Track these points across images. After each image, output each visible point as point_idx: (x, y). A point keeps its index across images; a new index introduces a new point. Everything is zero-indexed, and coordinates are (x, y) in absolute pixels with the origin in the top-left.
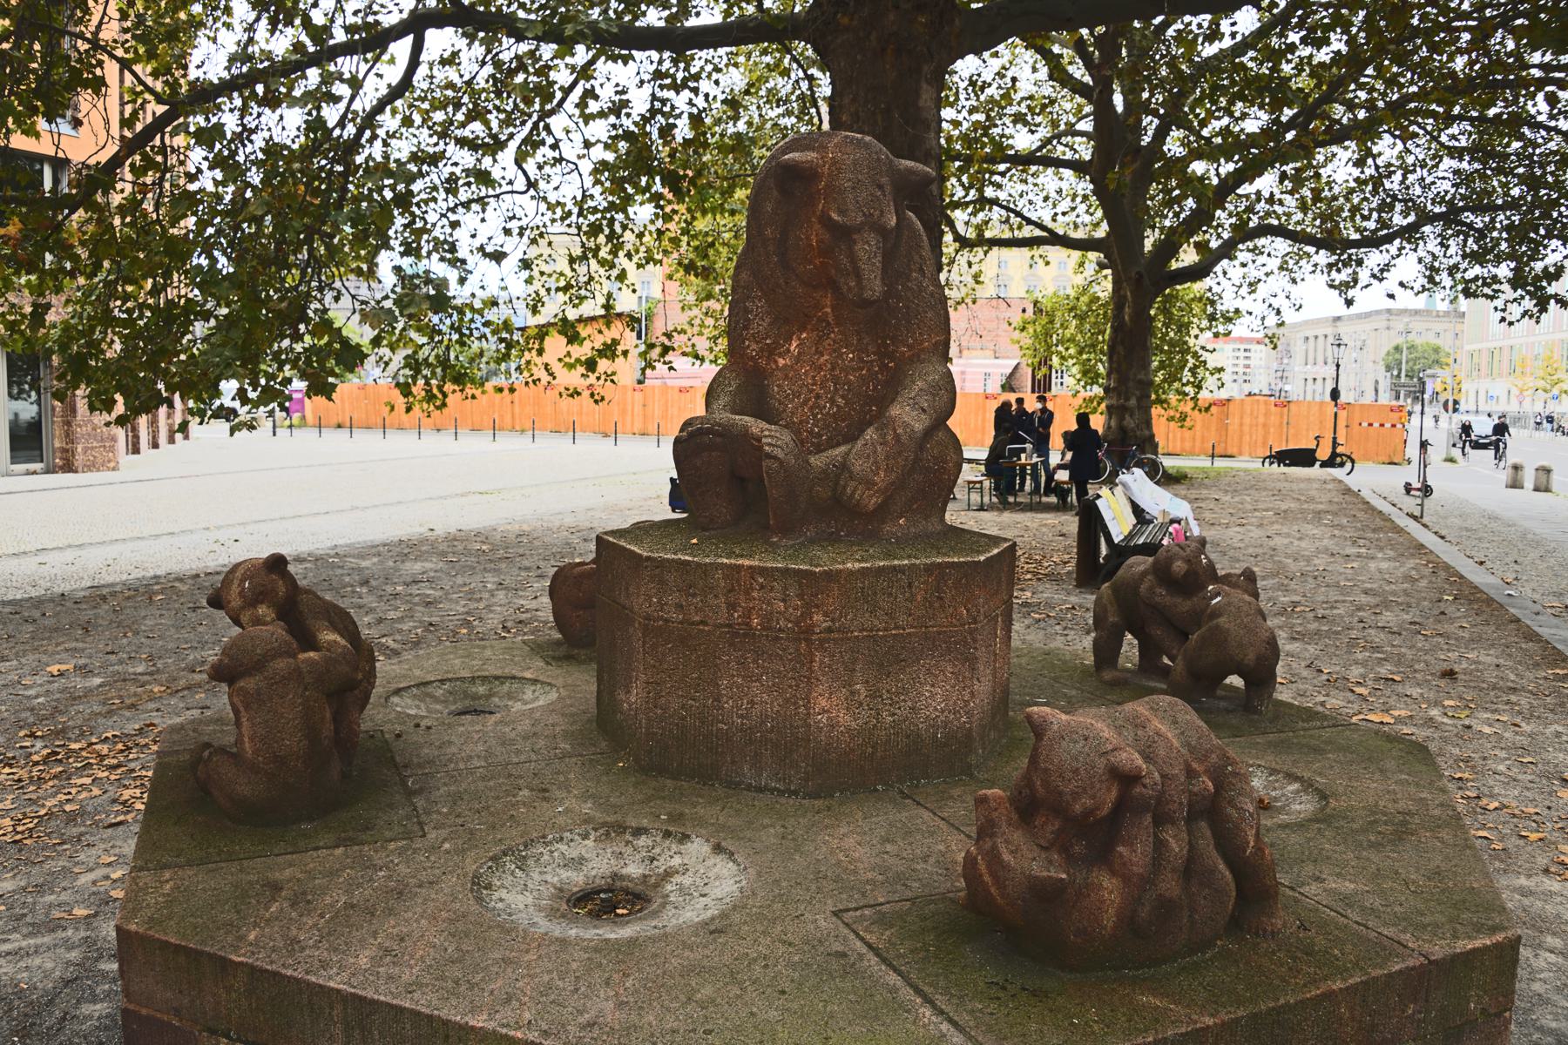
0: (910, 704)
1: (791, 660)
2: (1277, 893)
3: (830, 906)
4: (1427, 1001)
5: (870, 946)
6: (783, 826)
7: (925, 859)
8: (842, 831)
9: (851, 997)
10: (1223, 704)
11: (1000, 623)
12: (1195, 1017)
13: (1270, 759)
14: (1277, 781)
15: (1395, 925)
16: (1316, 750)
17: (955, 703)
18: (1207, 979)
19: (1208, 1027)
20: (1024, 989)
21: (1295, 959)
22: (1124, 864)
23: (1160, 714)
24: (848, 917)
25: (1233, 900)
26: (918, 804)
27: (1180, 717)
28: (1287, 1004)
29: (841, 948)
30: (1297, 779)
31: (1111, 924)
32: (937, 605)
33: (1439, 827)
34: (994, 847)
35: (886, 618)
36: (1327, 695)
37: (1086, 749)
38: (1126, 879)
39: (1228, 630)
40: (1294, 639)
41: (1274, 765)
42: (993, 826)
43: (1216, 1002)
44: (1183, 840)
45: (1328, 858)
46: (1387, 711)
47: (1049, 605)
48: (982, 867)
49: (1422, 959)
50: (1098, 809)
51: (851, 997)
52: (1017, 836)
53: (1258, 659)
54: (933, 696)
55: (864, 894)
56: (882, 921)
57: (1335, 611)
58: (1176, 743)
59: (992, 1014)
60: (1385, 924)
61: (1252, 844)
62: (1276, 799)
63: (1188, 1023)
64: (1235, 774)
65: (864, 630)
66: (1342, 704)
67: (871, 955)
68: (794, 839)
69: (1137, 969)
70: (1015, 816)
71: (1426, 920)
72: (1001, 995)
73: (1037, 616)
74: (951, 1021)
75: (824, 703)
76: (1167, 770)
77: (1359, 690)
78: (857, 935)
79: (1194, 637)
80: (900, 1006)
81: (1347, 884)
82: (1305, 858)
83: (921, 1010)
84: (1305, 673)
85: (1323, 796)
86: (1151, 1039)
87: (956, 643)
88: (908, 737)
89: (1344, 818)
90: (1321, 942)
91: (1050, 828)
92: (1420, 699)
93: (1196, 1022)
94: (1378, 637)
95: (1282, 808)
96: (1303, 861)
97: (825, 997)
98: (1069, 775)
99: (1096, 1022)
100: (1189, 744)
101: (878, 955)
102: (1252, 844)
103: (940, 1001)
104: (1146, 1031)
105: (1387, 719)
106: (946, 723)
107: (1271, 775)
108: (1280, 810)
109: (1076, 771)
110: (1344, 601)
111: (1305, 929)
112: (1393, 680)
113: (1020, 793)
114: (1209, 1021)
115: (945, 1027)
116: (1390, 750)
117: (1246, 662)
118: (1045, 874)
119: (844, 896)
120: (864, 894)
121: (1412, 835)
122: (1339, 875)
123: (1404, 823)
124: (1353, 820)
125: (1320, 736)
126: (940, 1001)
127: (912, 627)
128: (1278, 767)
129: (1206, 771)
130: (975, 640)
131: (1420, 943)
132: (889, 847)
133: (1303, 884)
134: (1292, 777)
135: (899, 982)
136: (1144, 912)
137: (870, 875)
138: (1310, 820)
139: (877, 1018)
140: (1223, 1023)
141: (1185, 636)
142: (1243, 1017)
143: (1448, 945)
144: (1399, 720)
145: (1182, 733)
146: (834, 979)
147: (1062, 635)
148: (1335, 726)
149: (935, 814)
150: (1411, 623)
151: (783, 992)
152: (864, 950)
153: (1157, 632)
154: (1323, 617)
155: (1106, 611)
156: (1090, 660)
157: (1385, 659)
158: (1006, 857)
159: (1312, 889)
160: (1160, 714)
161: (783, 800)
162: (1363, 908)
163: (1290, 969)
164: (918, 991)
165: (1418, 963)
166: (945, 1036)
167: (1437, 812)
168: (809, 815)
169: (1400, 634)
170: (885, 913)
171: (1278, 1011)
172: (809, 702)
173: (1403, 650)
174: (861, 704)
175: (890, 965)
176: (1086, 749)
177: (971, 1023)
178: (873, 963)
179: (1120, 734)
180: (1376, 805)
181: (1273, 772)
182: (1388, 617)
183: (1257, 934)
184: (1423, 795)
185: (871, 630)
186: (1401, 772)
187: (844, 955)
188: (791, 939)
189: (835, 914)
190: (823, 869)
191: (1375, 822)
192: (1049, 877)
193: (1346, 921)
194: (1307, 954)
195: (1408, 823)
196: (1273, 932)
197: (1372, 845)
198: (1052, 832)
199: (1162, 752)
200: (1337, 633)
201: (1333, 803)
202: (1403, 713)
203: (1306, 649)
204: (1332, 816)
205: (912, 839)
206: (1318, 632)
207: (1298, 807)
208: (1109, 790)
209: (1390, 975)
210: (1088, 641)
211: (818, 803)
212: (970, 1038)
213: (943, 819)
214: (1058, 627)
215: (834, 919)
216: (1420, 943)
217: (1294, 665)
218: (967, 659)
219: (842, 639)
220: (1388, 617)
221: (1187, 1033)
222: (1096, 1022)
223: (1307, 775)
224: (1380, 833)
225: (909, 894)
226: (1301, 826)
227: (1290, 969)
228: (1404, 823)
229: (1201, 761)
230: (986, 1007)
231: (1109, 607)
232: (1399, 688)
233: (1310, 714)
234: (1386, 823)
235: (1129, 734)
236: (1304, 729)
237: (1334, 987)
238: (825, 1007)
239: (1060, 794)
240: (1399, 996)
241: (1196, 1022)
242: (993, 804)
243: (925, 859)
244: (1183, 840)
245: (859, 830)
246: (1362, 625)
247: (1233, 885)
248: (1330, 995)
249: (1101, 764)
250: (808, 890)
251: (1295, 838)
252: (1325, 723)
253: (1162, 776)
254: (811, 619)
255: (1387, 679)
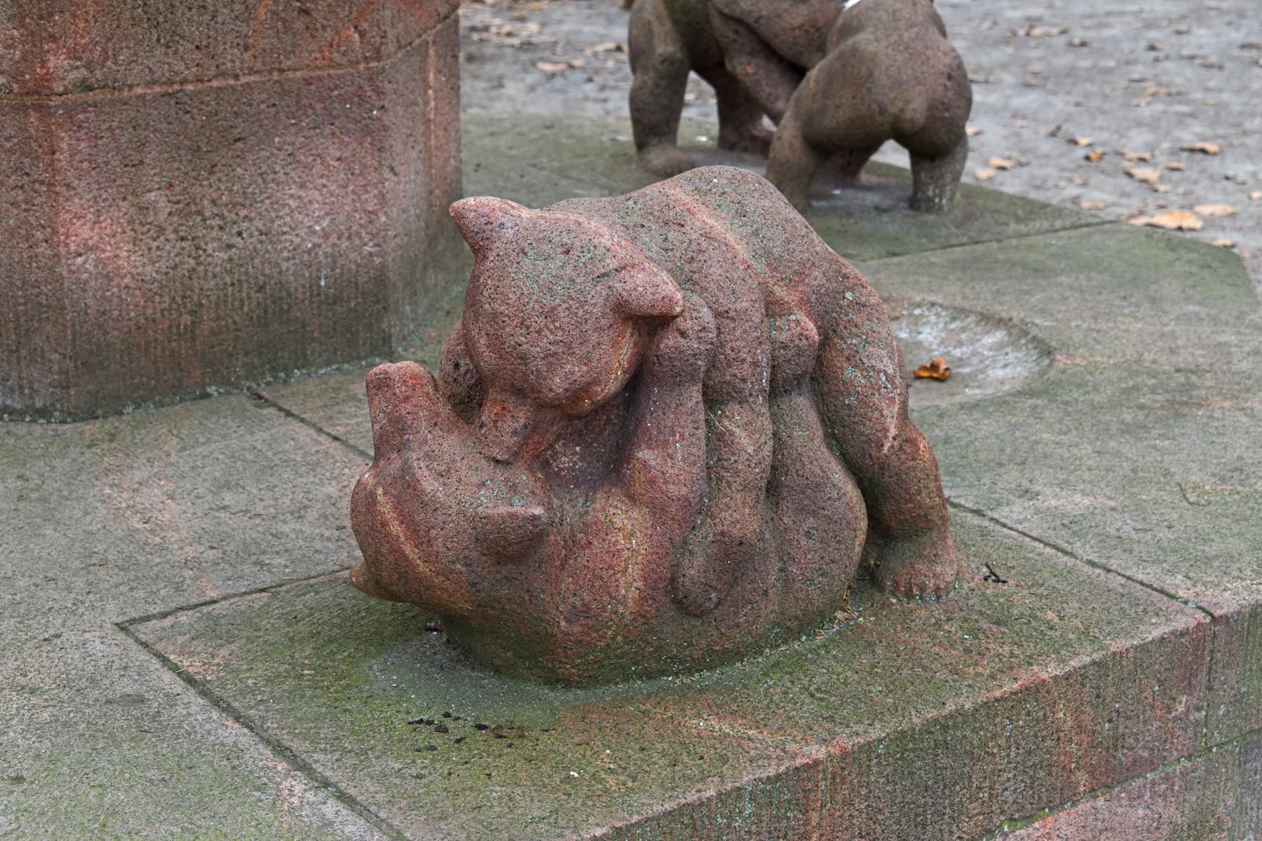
0: (259, 224)
1: (12, 151)
2: (944, 519)
3: (113, 614)
4: (1210, 688)
5: (190, 680)
6: (20, 477)
7: (299, 513)
8: (138, 475)
9: (153, 774)
10: (872, 199)
11: (432, 59)
12: (792, 747)
13: (953, 292)
14: (963, 329)
15: (1157, 561)
16: (1038, 271)
17: (349, 217)
18: (817, 680)
19: (817, 763)
20: (480, 727)
21: (975, 633)
22: (652, 482)
23: (713, 199)
24: (146, 631)
25: (862, 536)
26: (289, 414)
27: (751, 203)
28: (959, 712)
29: (131, 688)
30: (1001, 322)
31: (633, 593)
32: (299, 25)
33: (1248, 390)
34: (406, 469)
35: (197, 55)
36: (1085, 184)
37: (569, 269)
38: (657, 509)
39: (875, 55)
40: (1028, 86)
41: (959, 301)
42: (402, 431)
43: (831, 719)
44: (761, 431)
45: (1046, 456)
46: (1191, 207)
47: (573, 46)
48: (385, 507)
49: (1200, 615)
50: (596, 382)
51: (153, 774)
52: (451, 445)
53: (932, 107)
54: (303, 207)
55: (179, 589)
56: (215, 631)
57: (1106, 33)
58: (742, 251)
59: (419, 777)
60: (1143, 561)
61: (893, 431)
62: (961, 362)
63: (779, 759)
64: (860, 305)
65: (154, 82)
66: (1111, 199)
67: (191, 696)
68: (44, 500)
69: (690, 672)
70: (445, 410)
71: (1211, 550)
72: (437, 740)
73: (548, 67)
74: (342, 797)
75: (85, 232)
76: (725, 302)
77: (1142, 172)
78: (164, 660)
79: (813, 74)
80: (246, 780)
81: (1077, 498)
82: (1004, 459)
83: (286, 784)
84: (1046, 146)
85: (1047, 351)
86: (711, 792)
87: (343, 99)
88: (261, 288)
89: (1080, 386)
90: (1023, 601)
91: (509, 425)
92: (1251, 182)
93: (794, 756)
94: (1179, 75)
95: (972, 376)
96: (1000, 465)
97: (101, 778)
98: (538, 322)
99: (611, 771)
100: (768, 253)
101: (204, 694)
102: (893, 431)
103: (323, 763)
104: (703, 780)
105: (1190, 221)
106: (334, 259)
107: (954, 319)
108: (967, 381)
109: (550, 314)
110: (1123, 13)
111: (998, 580)
112: (1204, 151)
113: (457, 366)
114: (818, 752)
115: (331, 808)
116: (1171, 264)
117: (908, 115)
118: (503, 510)
119: (140, 594)
120: (179, 589)
121: (1200, 406)
122: (1063, 484)
123: (1188, 387)
124: (1096, 388)
125: (1047, 246)
126: (323, 763)
127: (252, 71)
128: (966, 305)
129: (803, 302)
130: (380, 93)
131: (1199, 588)
132: (229, 498)
133: (999, 504)
134: (990, 320)
135: (243, 737)
136: (694, 569)
137: (190, 552)
138: (1019, 393)
139: (202, 805)
140: (845, 755)
141: (797, 71)
142: (880, 741)
143: (1247, 588)
144: (1211, 222)
145: (756, 233)
146: (118, 746)
147: (596, 100)
148: (1075, 227)
149: (320, 430)
150: (1243, 47)
151: (19, 779)
152: (179, 686)
153: (747, 68)
154: (1083, 44)
155: (650, 34)
156: (626, 135)
157: (1192, 115)
158: (429, 484)
159: (1014, 512)
160: (713, 199)
161: (21, 429)
162: (1103, 538)
163: (967, 651)
164: (280, 749)
165: (1192, 623)
166: (331, 823)
167: (1245, 366)
168: (73, 452)
169: (1221, 68)
170: (218, 617)
171: (944, 725)
172: (55, 232)
173: (1225, 96)
174: (161, 230)
175: (228, 710)
176: (569, 269)
177: (380, 797)
178: (194, 708)
179: (634, 239)
180: (1139, 361)
181: (959, 313)
182: (1203, 39)
183: (909, 595)
184: (1223, 338)
185: (170, 82)
186: (1188, 299)
187: (140, 700)
188: (36, 682)
189: (122, 627)
190: (100, 548)
191: (1136, 388)
192: (513, 516)
193: (1070, 561)
194: (998, 623)
195: (1193, 386)
196: (937, 589)
197: (1126, 429)
198: (515, 433)
199: (716, 271)
200: (1108, 71)
201: (1061, 360)
202: (1219, 209)
203: (1049, 104)
204: (1058, 383)
205: (274, 481)
206: (1071, 72)
207: (1000, 373)
208: (615, 345)
209: (1143, 648)
210: (620, 105)
211: (90, 428)
212: (379, 823)
213: (336, 438)
214: (589, 88)
215: (121, 636)
216: (1199, 588)
217: (1027, 134)
218: (367, 131)
219: (112, 103)
220: (1203, 39)
221: (778, 777)
222: (611, 771)
223: (1017, 315)
224: (1142, 407)
225: (267, 579)
226: (1002, 403)
227: (967, 651)
228: (1188, 387)
229: (790, 284)
230: (408, 766)
231: (656, 28)
232: (1214, 165)
233: (1027, 209)
234: (1153, 390)
235: (651, 240)
236: (1021, 236)
237: (1044, 676)
238: (101, 796)
239: (524, 358)
240: (1160, 682)
241: (794, 756)
242: (400, 390)
243: (299, 513)
244: (761, 431)
245: (170, 471)
246: (1152, 54)
247: (861, 510)
248: (1034, 691)
249: (597, 297)
250: (69, 589)
251: (989, 426)
252: (1058, 223)
253: (718, 315)
254: (43, 64)
255: (1192, 150)
